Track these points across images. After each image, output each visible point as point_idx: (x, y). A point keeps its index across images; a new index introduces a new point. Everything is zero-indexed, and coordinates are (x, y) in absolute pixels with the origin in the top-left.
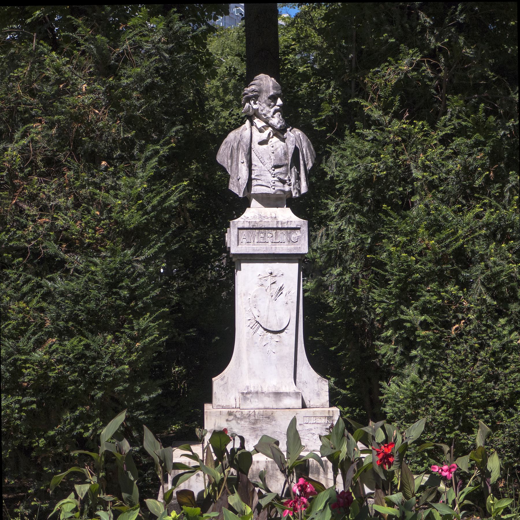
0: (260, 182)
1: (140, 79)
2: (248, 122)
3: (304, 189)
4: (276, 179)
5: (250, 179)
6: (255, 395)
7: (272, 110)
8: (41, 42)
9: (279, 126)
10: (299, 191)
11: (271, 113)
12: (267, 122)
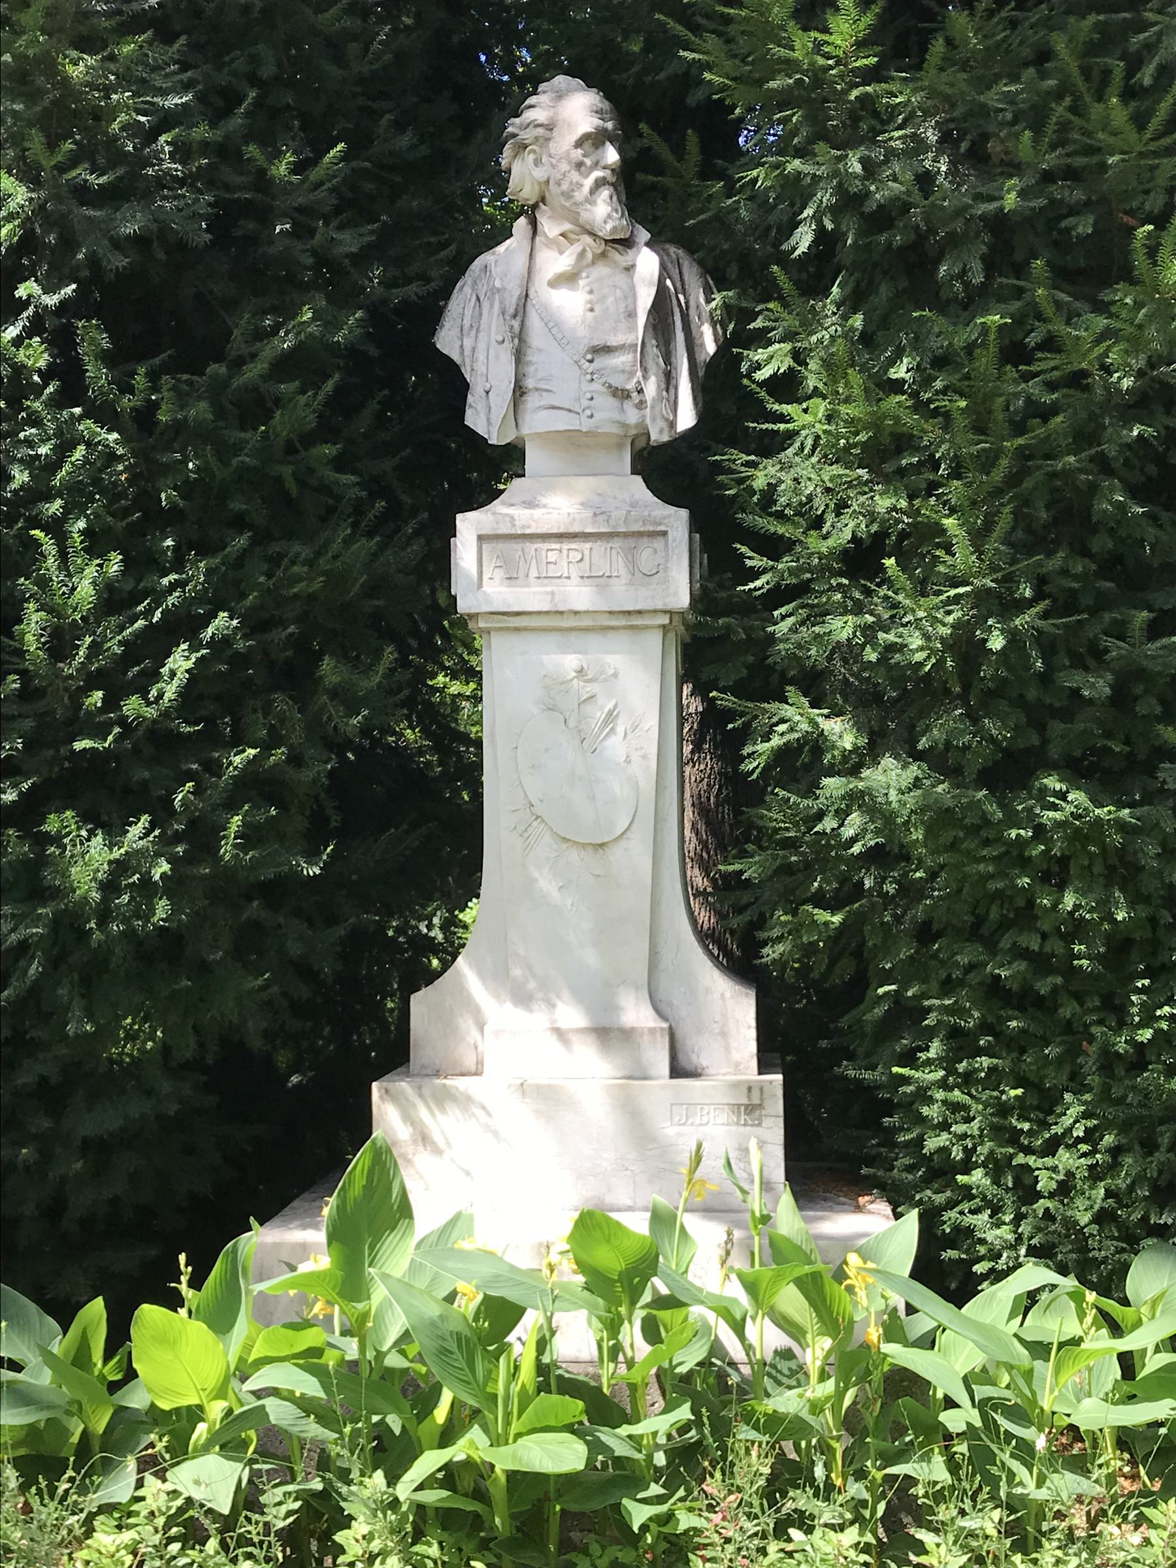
0: (547, 399)
1: (759, 1457)
2: (521, 225)
3: (686, 418)
4: (596, 386)
5: (519, 391)
6: (607, 1344)
7: (589, 182)
8: (593, 1384)
9: (609, 227)
10: (672, 424)
11: (586, 189)
12: (575, 221)
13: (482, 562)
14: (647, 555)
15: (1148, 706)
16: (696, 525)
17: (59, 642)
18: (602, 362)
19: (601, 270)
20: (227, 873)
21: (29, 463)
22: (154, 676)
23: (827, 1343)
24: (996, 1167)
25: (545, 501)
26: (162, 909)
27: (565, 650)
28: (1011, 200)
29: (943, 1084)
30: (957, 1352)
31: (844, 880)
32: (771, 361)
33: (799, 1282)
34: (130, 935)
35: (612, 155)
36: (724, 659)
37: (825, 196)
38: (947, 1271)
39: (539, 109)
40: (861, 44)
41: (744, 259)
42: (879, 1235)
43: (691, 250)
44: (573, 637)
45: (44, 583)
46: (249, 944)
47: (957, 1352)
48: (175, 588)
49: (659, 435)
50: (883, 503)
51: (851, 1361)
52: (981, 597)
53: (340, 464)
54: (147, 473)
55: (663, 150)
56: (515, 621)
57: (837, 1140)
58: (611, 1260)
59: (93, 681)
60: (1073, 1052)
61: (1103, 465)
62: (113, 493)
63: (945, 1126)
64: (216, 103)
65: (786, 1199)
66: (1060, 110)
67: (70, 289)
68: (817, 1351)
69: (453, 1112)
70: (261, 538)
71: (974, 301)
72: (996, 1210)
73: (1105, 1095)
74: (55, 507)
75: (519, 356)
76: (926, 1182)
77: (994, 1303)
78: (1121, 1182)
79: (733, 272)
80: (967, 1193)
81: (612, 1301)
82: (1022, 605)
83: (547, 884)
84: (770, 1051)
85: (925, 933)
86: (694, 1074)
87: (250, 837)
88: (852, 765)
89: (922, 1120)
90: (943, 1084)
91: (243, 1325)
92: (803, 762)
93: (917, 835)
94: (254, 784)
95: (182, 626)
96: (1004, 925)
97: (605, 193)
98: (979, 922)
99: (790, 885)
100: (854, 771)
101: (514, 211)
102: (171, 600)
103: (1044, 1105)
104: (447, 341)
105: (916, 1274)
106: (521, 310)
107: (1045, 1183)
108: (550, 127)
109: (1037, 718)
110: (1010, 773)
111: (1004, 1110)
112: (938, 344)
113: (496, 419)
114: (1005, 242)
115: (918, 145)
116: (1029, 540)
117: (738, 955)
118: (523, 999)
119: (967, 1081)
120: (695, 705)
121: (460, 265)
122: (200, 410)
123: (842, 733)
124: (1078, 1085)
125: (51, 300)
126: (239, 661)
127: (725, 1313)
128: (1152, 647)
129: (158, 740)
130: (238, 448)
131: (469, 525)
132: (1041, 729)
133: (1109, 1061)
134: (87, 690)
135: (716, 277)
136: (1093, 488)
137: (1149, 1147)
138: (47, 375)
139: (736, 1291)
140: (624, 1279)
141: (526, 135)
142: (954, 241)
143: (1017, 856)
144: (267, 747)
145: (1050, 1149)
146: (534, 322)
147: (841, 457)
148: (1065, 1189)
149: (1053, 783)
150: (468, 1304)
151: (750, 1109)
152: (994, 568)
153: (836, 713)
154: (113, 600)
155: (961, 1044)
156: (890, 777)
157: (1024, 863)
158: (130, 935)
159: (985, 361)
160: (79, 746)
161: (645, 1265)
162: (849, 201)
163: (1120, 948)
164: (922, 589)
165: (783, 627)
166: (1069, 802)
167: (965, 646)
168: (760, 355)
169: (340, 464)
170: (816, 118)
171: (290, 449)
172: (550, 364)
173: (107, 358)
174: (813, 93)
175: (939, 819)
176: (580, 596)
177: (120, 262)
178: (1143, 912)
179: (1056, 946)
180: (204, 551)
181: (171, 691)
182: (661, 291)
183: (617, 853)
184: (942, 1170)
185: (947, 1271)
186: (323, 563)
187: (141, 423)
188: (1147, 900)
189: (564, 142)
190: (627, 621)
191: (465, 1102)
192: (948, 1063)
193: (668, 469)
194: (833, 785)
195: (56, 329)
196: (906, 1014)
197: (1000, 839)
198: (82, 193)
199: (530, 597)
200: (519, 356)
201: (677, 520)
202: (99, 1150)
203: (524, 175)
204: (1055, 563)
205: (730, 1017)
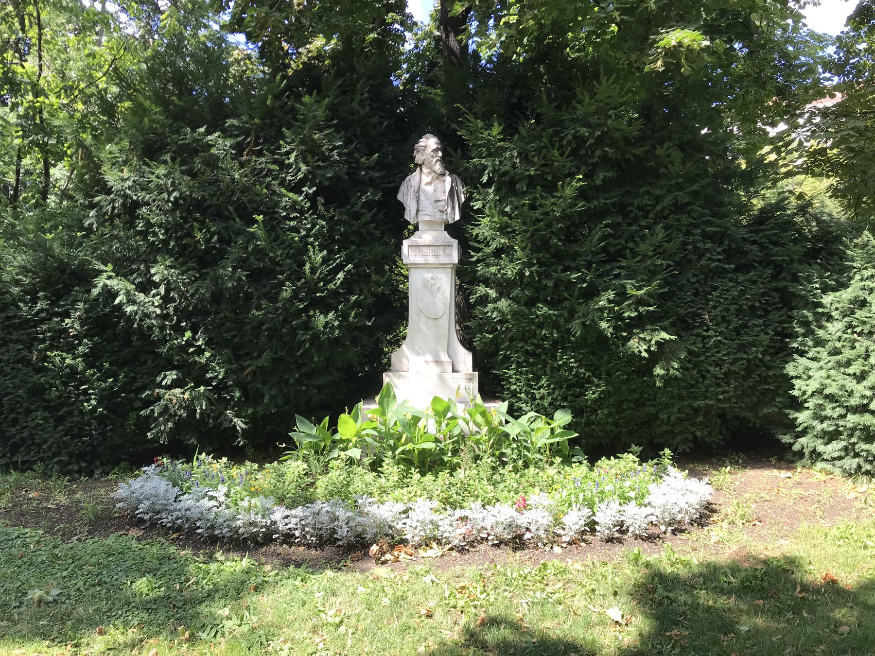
3: (457, 217)
5: (418, 210)
7: (434, 160)
13: (409, 252)
14: (448, 251)
15: (562, 288)
16: (459, 244)
17: (313, 270)
18: (438, 204)
19: (437, 181)
20: (350, 324)
21: (305, 229)
22: (333, 279)
23: (486, 428)
24: (527, 393)
25: (425, 237)
26: (337, 332)
27: (428, 272)
28: (532, 173)
29: (515, 374)
30: (514, 429)
31: (493, 327)
32: (478, 205)
33: (480, 413)
34: (329, 338)
35: (440, 154)
36: (465, 276)
37: (490, 168)
38: (514, 412)
39: (423, 142)
40: (499, 134)
41: (472, 178)
42: (499, 409)
43: (459, 176)
44: (431, 270)
45: (310, 257)
46: (355, 342)
47: (514, 429)
48: (339, 258)
49: (451, 221)
50: (503, 241)
51: (492, 430)
52: (524, 263)
53: (376, 228)
54: (332, 230)
55: (452, 152)
56: (416, 266)
57: (490, 388)
58: (440, 408)
59: (320, 280)
60: (544, 367)
61: (552, 233)
62: (324, 236)
63: (515, 384)
64: (347, 142)
65: (479, 397)
66: (544, 151)
67: (315, 188)
68: (485, 429)
69: (402, 379)
70: (358, 246)
71: (524, 194)
72: (527, 403)
73: (552, 377)
74: (312, 239)
75: (418, 202)
76: (511, 397)
77: (524, 419)
78: (555, 396)
79: (469, 181)
80: (520, 399)
81: (440, 417)
82: (534, 265)
83: (423, 327)
84: (476, 366)
85: (512, 340)
86: (457, 372)
87: (356, 316)
88: (495, 301)
89: (511, 383)
90: (515, 374)
91: (360, 421)
92: (484, 300)
93: (509, 317)
94: (357, 304)
95: (339, 268)
96: (529, 338)
97: (439, 163)
98: (524, 336)
99: (480, 329)
100: (496, 302)
101: (416, 166)
102: (338, 261)
103: (538, 379)
104: (400, 197)
105: (507, 413)
106: (418, 191)
107: (538, 396)
108: (425, 147)
109: (537, 290)
110: (531, 303)
111: (529, 380)
112: (516, 204)
113: (412, 217)
114: (532, 182)
115: (512, 157)
116: (536, 249)
117: (467, 344)
118: (418, 354)
119: (521, 373)
120: (458, 282)
121: (403, 179)
122: (345, 217)
123: (493, 293)
124: (545, 374)
125: (311, 191)
126: (352, 275)
127: (464, 420)
128: (563, 275)
129: (335, 293)
130: (353, 225)
131: (406, 243)
132: (538, 292)
133: (553, 369)
134: (319, 282)
135: (465, 183)
136: (550, 238)
137: (561, 388)
138: (309, 209)
139: (468, 417)
140: (442, 413)
141: (420, 149)
142: (521, 180)
143: (532, 322)
144: (359, 295)
145: (539, 388)
146: (422, 197)
147: (494, 229)
148: (542, 398)
149: (540, 305)
150: (409, 417)
151: (470, 379)
152: (527, 256)
153: (491, 288)
154: (325, 261)
155: (519, 365)
156: (503, 304)
157: (534, 323)
158: (329, 338)
159: (526, 208)
160: (318, 295)
161: (447, 409)
162: (494, 171)
163: (556, 343)
164: (511, 261)
165: (479, 269)
166: (543, 310)
167: (521, 274)
168: (475, 203)
169: (376, 228)
170: (488, 150)
171: (364, 225)
172: (425, 202)
173: (323, 205)
174: (488, 144)
175: (514, 313)
176: (431, 260)
177: (327, 183)
178: (561, 334)
179: (541, 342)
180: (345, 249)
181: (339, 283)
182: (452, 186)
183: (440, 321)
184: (514, 394)
185: (514, 412)
186: (372, 252)
187: (330, 220)
188: (561, 332)
189: (429, 150)
190: (443, 266)
191: (404, 377)
192: (516, 369)
193: (453, 229)
194: (490, 306)
195: (312, 198)
196: (507, 358)
197: (528, 318)
198: (319, 167)
199: (419, 260)
200: (418, 202)
201: (455, 242)
202: (320, 388)
203: (419, 158)
204: (541, 255)
205: (465, 359)
